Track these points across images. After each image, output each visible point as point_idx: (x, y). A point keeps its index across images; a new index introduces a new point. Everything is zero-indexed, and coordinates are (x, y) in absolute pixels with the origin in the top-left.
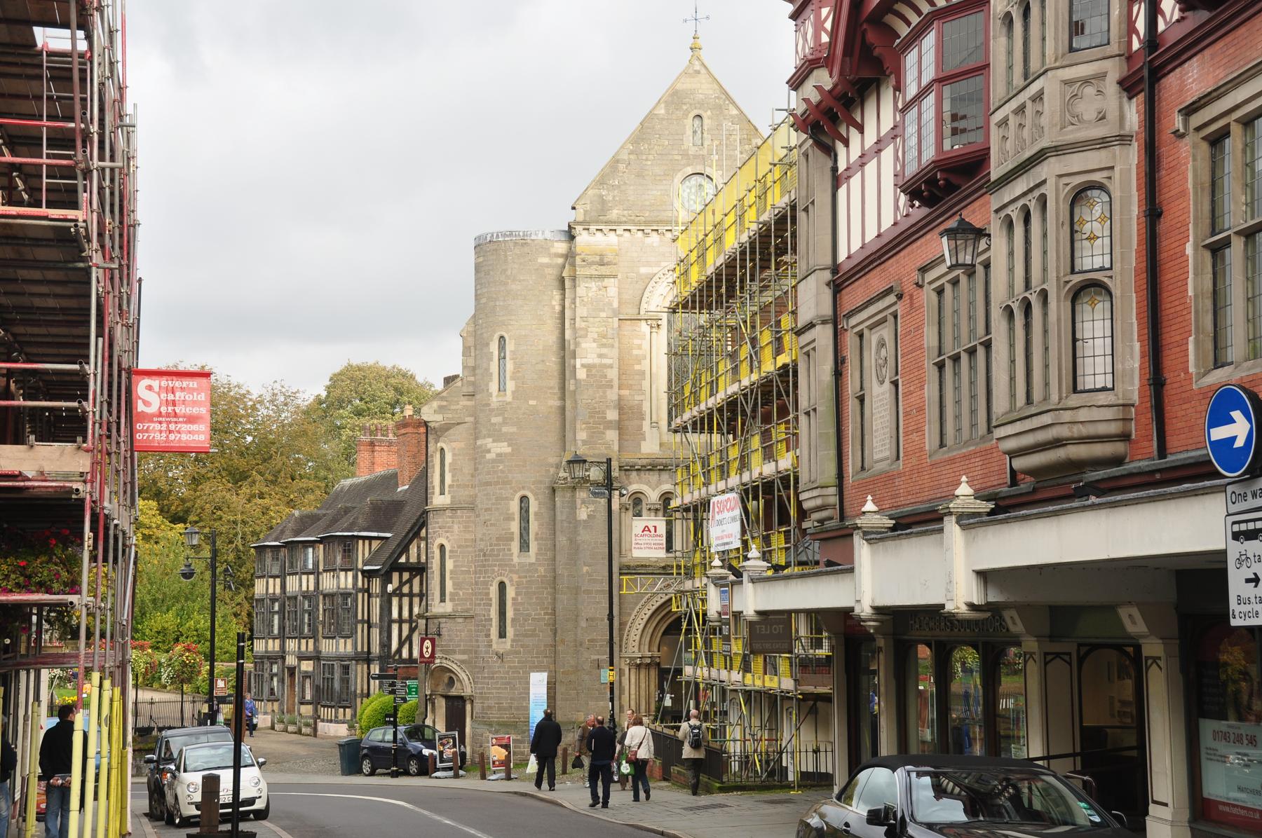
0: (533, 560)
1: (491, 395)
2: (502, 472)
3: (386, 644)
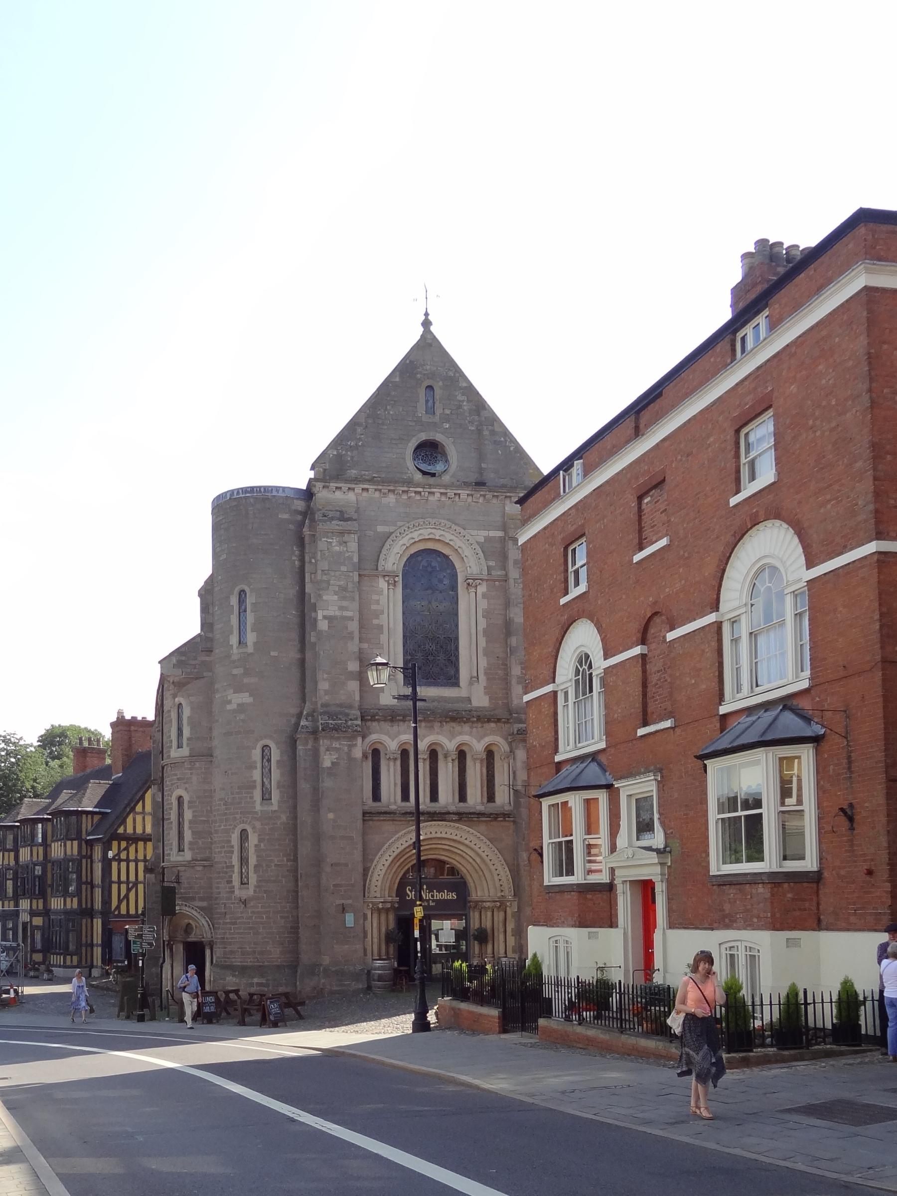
2: (243, 721)
3: (107, 901)
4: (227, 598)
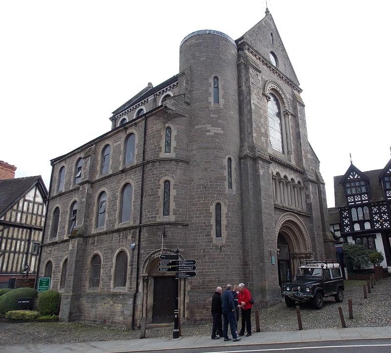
1: (210, 103)
4: (207, 79)
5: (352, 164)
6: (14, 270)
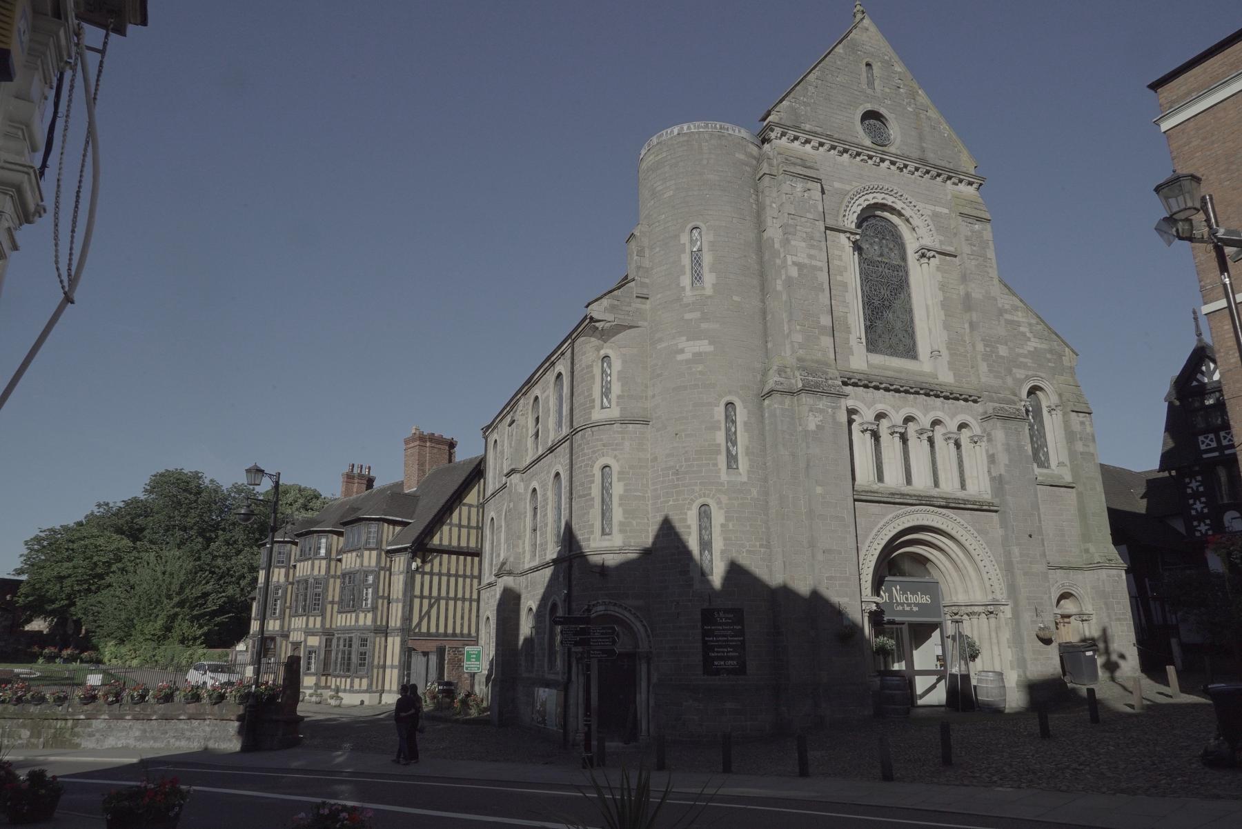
0: (745, 479)
4: (677, 237)
5: (1200, 340)
6: (450, 631)
